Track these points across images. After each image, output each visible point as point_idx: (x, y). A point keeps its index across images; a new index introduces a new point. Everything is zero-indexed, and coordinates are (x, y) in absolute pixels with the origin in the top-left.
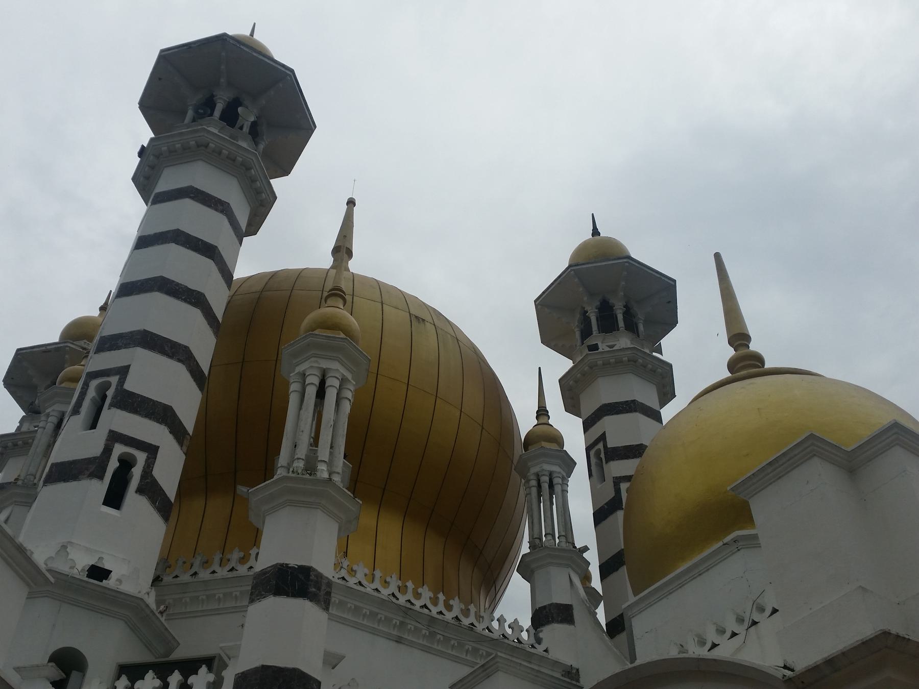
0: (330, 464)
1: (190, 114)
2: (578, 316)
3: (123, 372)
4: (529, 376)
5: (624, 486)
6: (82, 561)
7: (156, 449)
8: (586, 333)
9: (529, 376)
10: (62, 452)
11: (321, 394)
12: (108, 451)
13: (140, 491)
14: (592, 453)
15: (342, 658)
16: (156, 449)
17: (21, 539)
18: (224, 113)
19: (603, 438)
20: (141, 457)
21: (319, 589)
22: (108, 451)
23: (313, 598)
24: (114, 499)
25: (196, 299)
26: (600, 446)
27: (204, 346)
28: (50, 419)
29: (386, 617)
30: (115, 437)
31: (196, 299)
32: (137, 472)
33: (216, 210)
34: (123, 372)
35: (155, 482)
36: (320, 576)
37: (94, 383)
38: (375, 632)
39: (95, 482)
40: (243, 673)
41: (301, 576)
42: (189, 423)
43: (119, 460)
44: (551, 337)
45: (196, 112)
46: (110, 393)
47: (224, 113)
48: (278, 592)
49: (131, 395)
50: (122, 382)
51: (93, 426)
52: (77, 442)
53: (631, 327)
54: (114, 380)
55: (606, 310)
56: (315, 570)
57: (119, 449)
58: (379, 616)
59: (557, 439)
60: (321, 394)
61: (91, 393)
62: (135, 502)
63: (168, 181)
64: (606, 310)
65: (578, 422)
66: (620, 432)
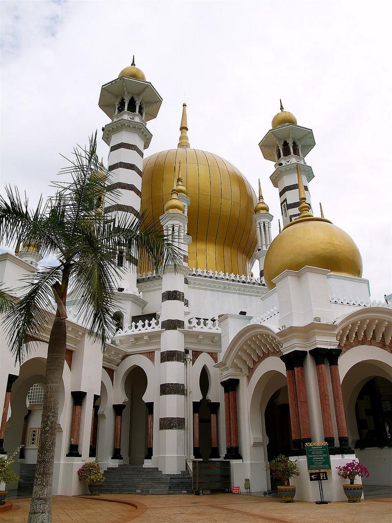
1: (117, 110)
2: (119, 100)
4: (258, 172)
8: (279, 156)
9: (258, 172)
11: (264, 228)
14: (283, 206)
18: (129, 99)
19: (285, 200)
25: (131, 187)
26: (285, 203)
27: (137, 182)
30: (291, 217)
31: (131, 187)
44: (267, 156)
45: (119, 110)
47: (129, 99)
48: (169, 299)
53: (296, 152)
55: (286, 144)
60: (264, 228)
62: (126, 263)
63: (116, 139)
64: (286, 144)
65: (277, 191)
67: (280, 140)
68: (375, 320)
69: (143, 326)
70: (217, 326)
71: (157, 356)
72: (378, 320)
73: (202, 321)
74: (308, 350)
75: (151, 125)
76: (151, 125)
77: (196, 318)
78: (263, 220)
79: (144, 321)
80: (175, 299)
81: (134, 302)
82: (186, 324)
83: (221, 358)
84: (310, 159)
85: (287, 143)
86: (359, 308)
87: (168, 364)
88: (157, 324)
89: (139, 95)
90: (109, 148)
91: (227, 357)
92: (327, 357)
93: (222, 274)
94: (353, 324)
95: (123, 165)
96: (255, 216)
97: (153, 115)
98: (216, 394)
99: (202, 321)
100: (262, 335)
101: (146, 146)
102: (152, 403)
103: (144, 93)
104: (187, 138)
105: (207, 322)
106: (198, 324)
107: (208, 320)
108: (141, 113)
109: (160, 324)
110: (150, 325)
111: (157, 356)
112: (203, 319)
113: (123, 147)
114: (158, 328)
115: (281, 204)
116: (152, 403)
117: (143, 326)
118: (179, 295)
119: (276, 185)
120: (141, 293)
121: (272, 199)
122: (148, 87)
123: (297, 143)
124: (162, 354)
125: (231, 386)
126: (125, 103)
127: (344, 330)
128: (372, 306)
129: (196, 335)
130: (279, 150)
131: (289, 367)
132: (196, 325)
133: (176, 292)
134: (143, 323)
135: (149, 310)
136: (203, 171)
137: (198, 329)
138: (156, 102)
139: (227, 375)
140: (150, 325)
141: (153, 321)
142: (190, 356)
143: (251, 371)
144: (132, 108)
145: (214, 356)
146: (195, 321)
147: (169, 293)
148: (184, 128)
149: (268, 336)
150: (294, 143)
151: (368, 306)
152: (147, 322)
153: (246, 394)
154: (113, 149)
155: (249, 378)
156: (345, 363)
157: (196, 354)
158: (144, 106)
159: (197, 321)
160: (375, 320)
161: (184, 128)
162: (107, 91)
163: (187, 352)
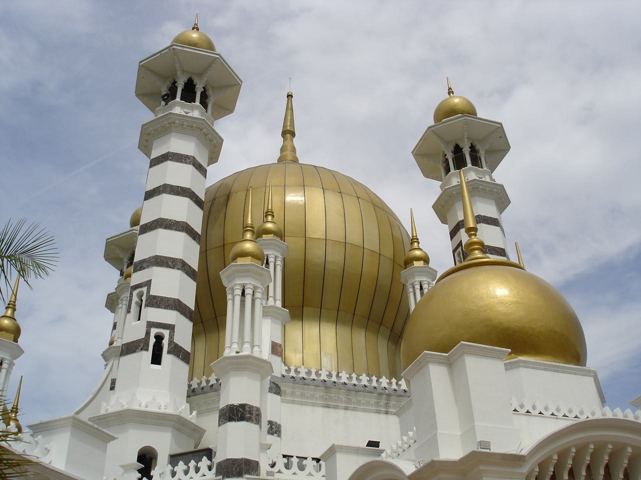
0: (275, 300)
3: (148, 284)
4: (413, 202)
7: (174, 326)
9: (413, 202)
10: (129, 338)
12: (148, 333)
13: (169, 352)
14: (456, 254)
15: (271, 445)
16: (174, 326)
17: (214, 128)
20: (166, 333)
21: (252, 414)
22: (148, 333)
23: (249, 420)
24: (156, 359)
27: (195, 217)
28: (124, 302)
29: (320, 396)
30: (151, 325)
31: (185, 228)
32: (165, 342)
33: (186, 163)
34: (148, 284)
35: (176, 346)
36: (251, 407)
37: (135, 293)
38: (313, 405)
39: (144, 352)
40: (219, 463)
41: (241, 409)
43: (155, 337)
46: (144, 298)
48: (231, 419)
49: (155, 297)
50: (148, 291)
52: (134, 330)
53: (476, 162)
54: (145, 289)
55: (458, 150)
56: (247, 405)
57: (154, 331)
58: (316, 396)
61: (135, 299)
64: (458, 150)
65: (446, 229)
67: (447, 143)
68: (586, 446)
69: (186, 472)
72: (593, 442)
73: (295, 461)
75: (224, 127)
76: (224, 127)
77: (284, 456)
79: (187, 463)
80: (242, 418)
81: (178, 430)
82: (264, 467)
84: (505, 173)
85: (461, 147)
86: (562, 424)
89: (200, 75)
90: (148, 161)
93: (364, 379)
94: (562, 455)
95: (168, 189)
96: (404, 273)
97: (227, 109)
99: (295, 461)
101: (213, 158)
103: (209, 72)
104: (294, 150)
105: (305, 462)
106: (287, 466)
107: (306, 458)
108: (204, 103)
110: (197, 470)
112: (297, 457)
113: (171, 160)
115: (454, 251)
117: (186, 472)
118: (250, 412)
119: (444, 220)
120: (194, 413)
122: (218, 63)
123: (478, 147)
126: (177, 88)
128: (591, 418)
130: (447, 160)
132: (283, 469)
133: (243, 406)
134: (185, 467)
135: (204, 444)
138: (231, 86)
140: (197, 470)
144: (189, 94)
148: (288, 133)
150: (472, 147)
151: (583, 418)
152: (192, 463)
154: (155, 162)
158: (210, 92)
159: (285, 460)
160: (586, 446)
161: (288, 133)
162: (147, 69)
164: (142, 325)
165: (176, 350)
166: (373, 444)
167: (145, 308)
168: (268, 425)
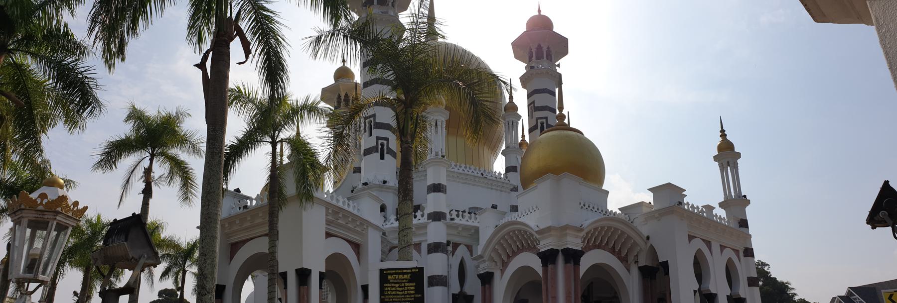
3: (374, 116)
4: (509, 69)
5: (539, 121)
6: (382, 179)
9: (509, 69)
12: (377, 143)
19: (533, 102)
20: (385, 142)
22: (377, 143)
24: (382, 157)
30: (378, 138)
32: (385, 147)
34: (374, 116)
42: (394, 124)
44: (518, 56)
48: (434, 191)
51: (371, 135)
54: (372, 119)
59: (515, 108)
66: (541, 100)
70: (473, 219)
71: (424, 248)
73: (461, 213)
74: (560, 248)
78: (512, 119)
80: (439, 191)
82: (448, 216)
83: (479, 250)
87: (434, 255)
88: (422, 216)
91: (485, 250)
92: (573, 256)
94: (595, 229)
98: (473, 287)
99: (461, 213)
100: (520, 231)
102: (286, 273)
106: (458, 216)
109: (426, 216)
111: (424, 248)
114: (424, 220)
116: (286, 273)
121: (521, 99)
124: (429, 245)
125: (487, 279)
127: (587, 234)
129: (456, 227)
131: (545, 264)
133: (440, 184)
136: (476, 64)
137: (457, 221)
139: (484, 268)
141: (419, 213)
142: (450, 248)
143: (505, 265)
145: (470, 248)
146: (454, 213)
147: (434, 185)
149: (526, 232)
153: (500, 285)
155: (502, 272)
156: (586, 262)
157: (456, 246)
163: (448, 243)
164: (374, 138)
165: (390, 152)
166: (385, 182)
167: (110, 66)
168: (620, 209)
